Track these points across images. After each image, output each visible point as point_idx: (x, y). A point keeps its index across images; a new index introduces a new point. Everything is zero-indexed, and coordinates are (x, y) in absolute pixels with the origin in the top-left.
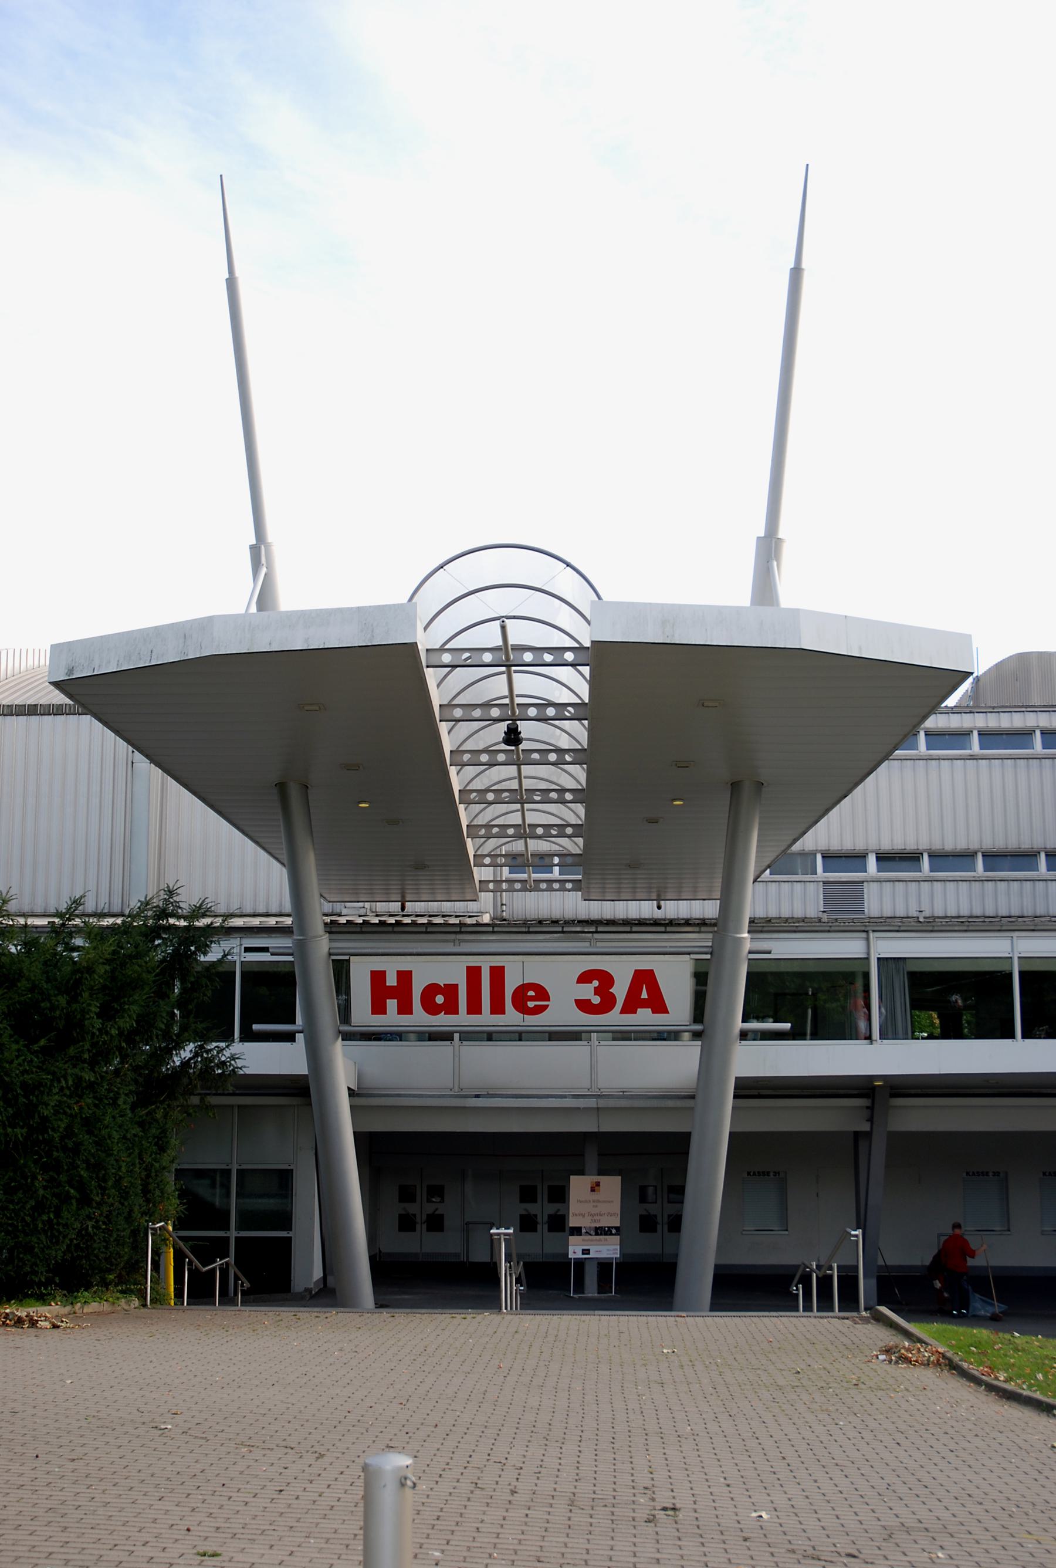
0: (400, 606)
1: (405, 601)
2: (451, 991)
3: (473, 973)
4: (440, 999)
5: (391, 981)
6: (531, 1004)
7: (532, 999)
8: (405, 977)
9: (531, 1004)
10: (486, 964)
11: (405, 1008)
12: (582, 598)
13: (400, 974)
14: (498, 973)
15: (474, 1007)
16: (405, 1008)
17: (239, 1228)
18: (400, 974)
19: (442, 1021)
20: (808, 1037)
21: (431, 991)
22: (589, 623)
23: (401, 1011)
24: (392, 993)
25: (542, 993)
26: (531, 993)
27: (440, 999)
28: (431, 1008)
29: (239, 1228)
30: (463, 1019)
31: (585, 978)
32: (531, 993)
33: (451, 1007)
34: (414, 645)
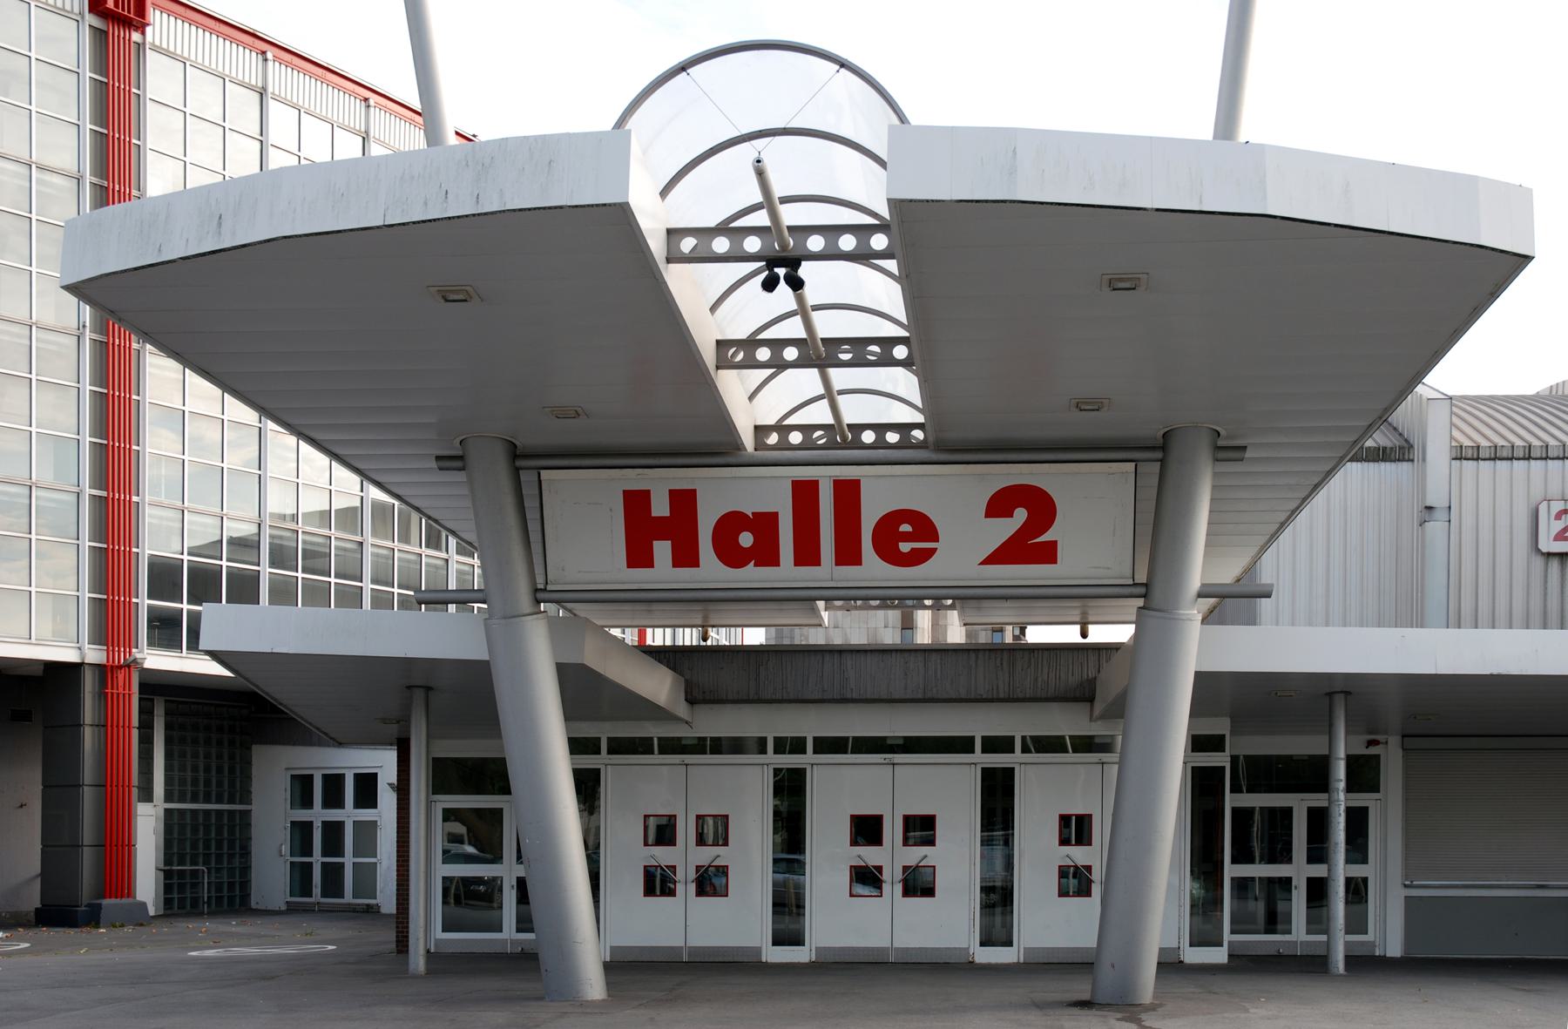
0: (597, 137)
1: (608, 124)
2: (765, 524)
3: (805, 493)
4: (746, 540)
5: (660, 508)
6: (905, 547)
7: (907, 537)
8: (684, 501)
9: (905, 547)
10: (825, 476)
11: (686, 556)
12: (871, 126)
13: (674, 494)
14: (848, 493)
15: (807, 554)
16: (686, 556)
17: (189, 611)
18: (674, 494)
19: (752, 575)
20: (780, 877)
21: (730, 524)
22: (882, 163)
23: (677, 563)
24: (661, 528)
25: (925, 528)
26: (906, 528)
27: (746, 540)
28: (730, 555)
29: (189, 611)
30: (787, 572)
31: (999, 505)
32: (906, 528)
33: (766, 554)
34: (621, 215)
